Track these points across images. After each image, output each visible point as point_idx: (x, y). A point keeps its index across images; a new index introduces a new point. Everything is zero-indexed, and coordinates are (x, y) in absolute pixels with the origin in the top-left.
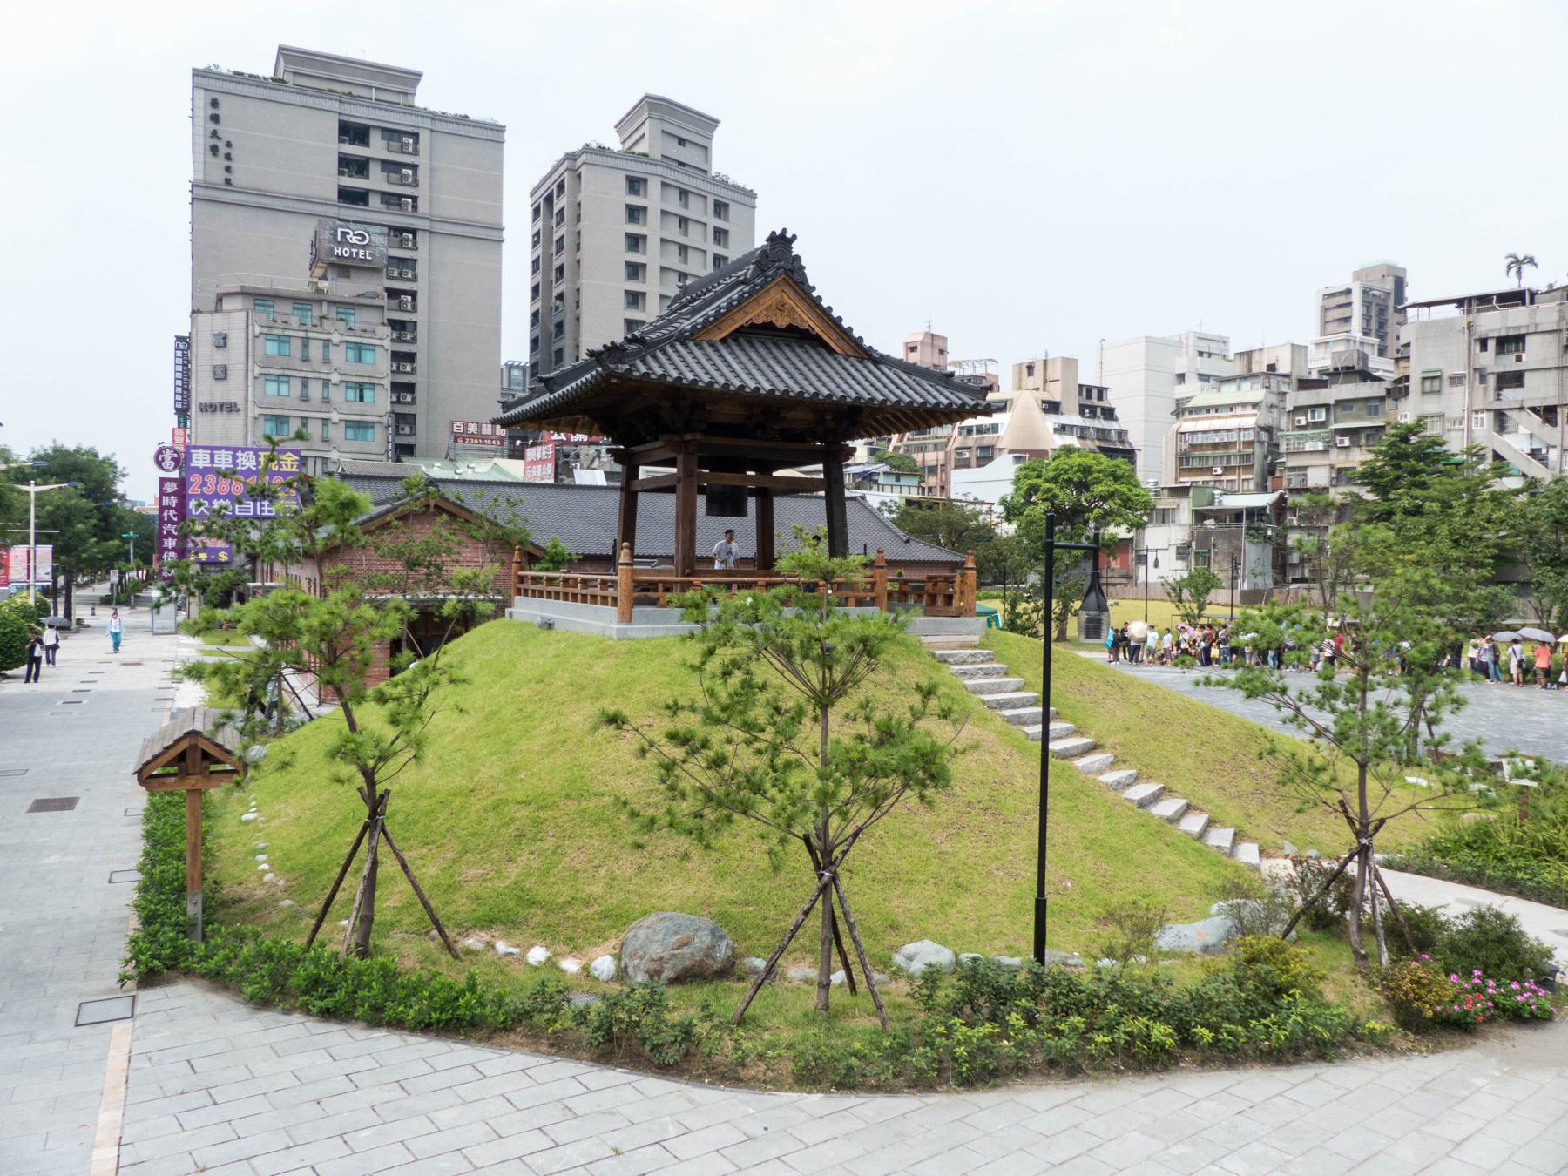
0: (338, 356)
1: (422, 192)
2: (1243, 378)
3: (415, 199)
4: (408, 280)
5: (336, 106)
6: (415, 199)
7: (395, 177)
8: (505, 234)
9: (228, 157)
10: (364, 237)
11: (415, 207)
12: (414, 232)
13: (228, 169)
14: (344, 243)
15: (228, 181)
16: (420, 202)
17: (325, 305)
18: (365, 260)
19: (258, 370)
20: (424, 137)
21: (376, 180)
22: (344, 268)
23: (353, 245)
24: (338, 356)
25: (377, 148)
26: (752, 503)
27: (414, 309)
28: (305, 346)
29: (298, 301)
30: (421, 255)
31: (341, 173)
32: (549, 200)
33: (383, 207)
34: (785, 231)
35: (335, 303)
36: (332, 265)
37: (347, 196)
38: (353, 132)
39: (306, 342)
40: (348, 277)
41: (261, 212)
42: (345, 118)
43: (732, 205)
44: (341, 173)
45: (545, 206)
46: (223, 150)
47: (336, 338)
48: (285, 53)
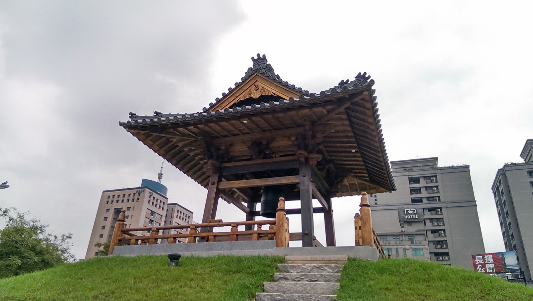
1: (441, 194)
3: (439, 197)
5: (407, 174)
6: (439, 197)
7: (430, 191)
10: (414, 211)
11: (439, 200)
12: (441, 208)
13: (376, 200)
14: (408, 214)
15: (376, 204)
16: (441, 197)
17: (404, 236)
18: (416, 219)
20: (439, 176)
21: (424, 194)
22: (409, 222)
23: (411, 214)
25: (423, 183)
27: (445, 236)
28: (397, 251)
29: (395, 236)
30: (444, 216)
31: (411, 194)
32: (498, 189)
33: (428, 202)
34: (365, 73)
35: (407, 235)
36: (405, 222)
37: (414, 201)
39: (397, 249)
40: (411, 225)
41: (387, 211)
44: (411, 194)
45: (496, 190)
47: (407, 247)
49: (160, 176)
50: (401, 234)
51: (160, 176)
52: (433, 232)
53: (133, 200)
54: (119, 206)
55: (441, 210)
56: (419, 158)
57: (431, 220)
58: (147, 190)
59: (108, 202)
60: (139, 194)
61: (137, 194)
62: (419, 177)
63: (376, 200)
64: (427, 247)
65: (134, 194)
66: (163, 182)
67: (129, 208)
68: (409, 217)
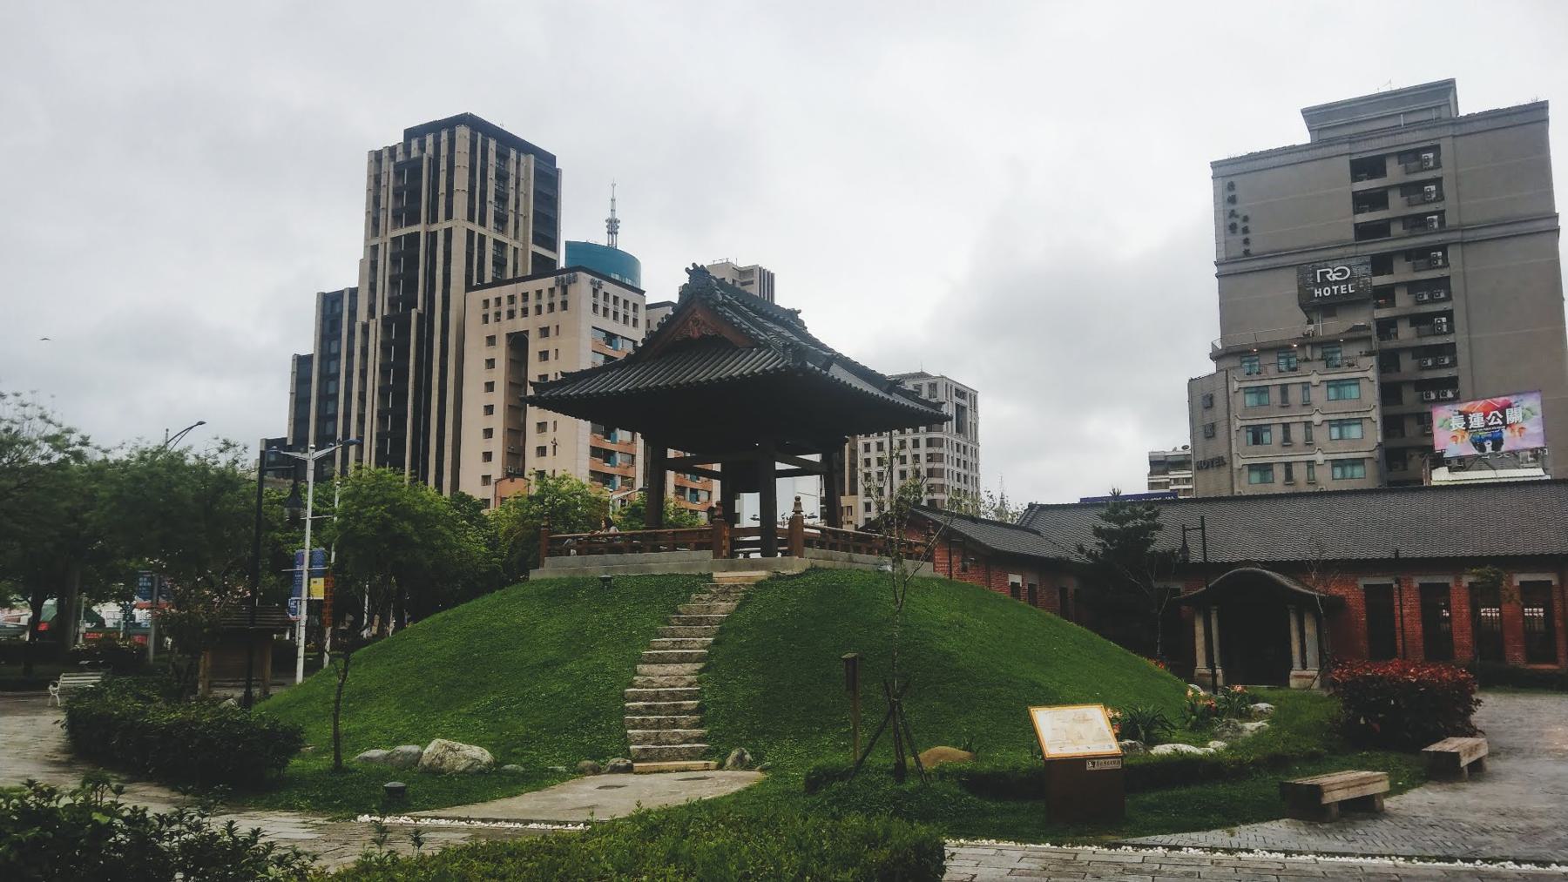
2: (517, 381)
3: (1441, 213)
5: (1346, 148)
6: (1441, 213)
7: (1416, 197)
8: (1215, 270)
9: (1246, 230)
11: (1442, 222)
12: (1443, 248)
13: (1246, 241)
14: (1326, 282)
19: (1239, 423)
20: (1446, 146)
21: (1397, 205)
22: (1329, 307)
23: (1336, 283)
24: (1318, 396)
25: (1395, 172)
31: (1356, 212)
42: (1355, 157)
46: (1240, 225)
47: (1315, 379)
48: (1313, 116)
49: (613, 227)
50: (1307, 341)
51: (613, 227)
53: (551, 307)
54: (519, 324)
55: (1445, 254)
56: (1396, 87)
57: (1412, 287)
58: (584, 278)
59: (486, 318)
60: (565, 292)
61: (558, 291)
63: (1246, 241)
64: (1372, 374)
65: (552, 290)
66: (624, 244)
67: (545, 332)
68: (1327, 292)
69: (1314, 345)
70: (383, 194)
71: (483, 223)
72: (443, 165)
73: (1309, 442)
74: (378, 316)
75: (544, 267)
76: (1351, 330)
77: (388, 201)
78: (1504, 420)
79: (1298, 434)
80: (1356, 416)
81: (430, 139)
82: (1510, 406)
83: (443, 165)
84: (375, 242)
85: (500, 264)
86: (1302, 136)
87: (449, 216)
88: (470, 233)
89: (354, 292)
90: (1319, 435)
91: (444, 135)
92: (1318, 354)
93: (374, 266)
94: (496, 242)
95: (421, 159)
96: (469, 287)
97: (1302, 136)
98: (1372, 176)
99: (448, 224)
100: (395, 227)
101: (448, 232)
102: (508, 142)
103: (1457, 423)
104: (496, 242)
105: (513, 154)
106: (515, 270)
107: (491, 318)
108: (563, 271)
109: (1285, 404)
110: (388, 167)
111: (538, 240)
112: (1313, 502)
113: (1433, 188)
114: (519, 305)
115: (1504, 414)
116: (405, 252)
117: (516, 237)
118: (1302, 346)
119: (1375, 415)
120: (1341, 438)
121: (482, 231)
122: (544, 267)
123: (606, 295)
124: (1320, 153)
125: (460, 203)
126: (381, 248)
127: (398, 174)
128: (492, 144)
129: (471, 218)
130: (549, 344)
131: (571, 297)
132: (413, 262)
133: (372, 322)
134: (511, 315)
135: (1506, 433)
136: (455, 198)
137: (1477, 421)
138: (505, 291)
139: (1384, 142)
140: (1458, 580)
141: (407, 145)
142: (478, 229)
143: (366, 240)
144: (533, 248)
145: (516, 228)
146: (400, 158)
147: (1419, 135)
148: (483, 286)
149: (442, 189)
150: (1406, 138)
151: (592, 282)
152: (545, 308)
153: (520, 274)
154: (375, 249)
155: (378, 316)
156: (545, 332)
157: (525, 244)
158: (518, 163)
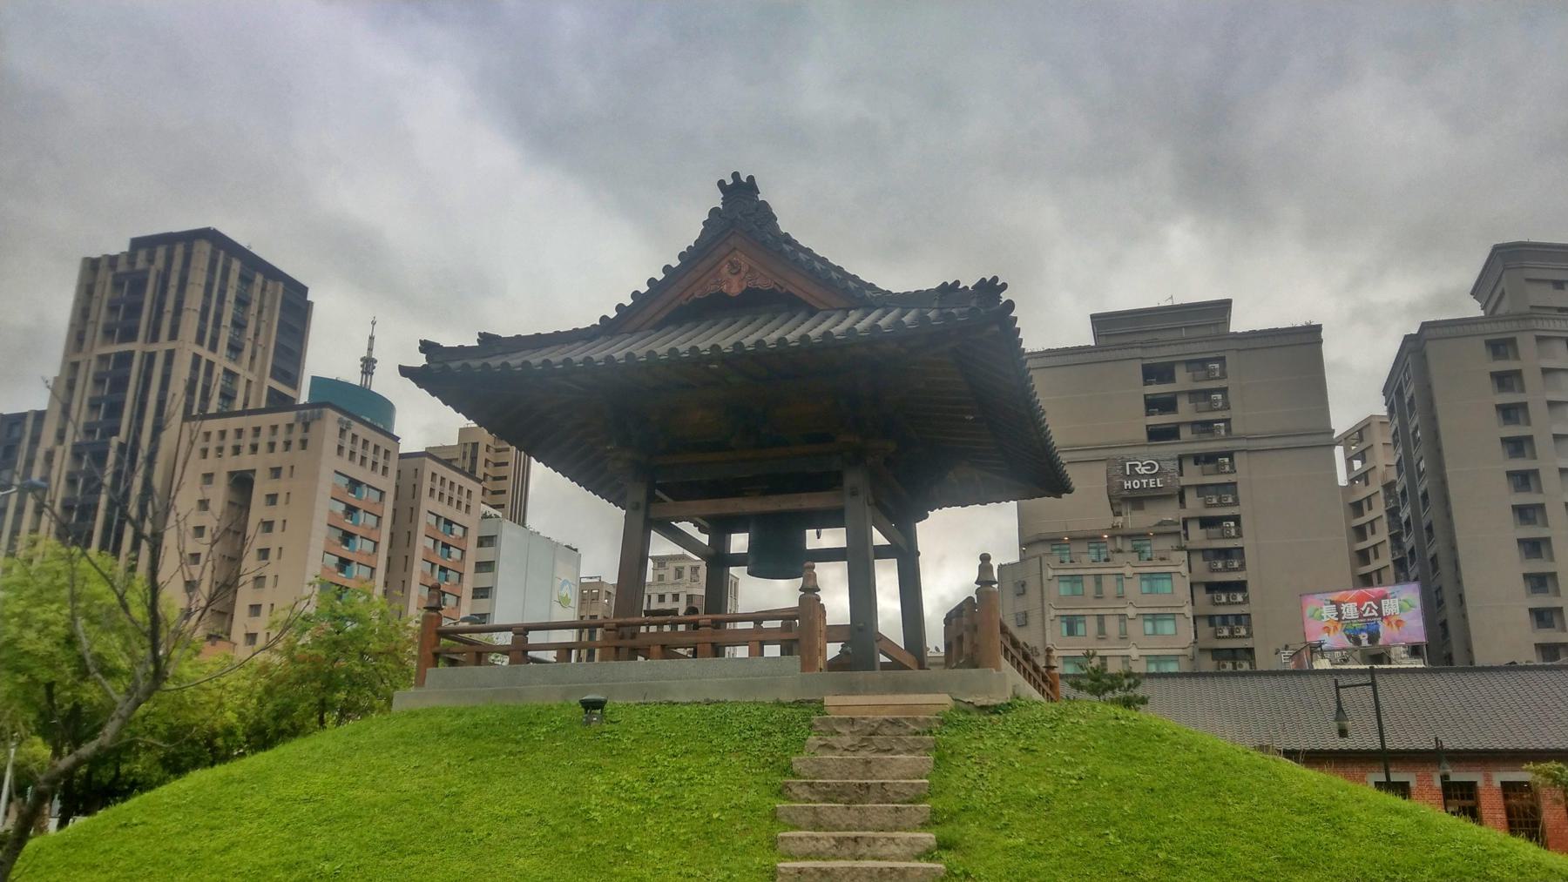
0: (1133, 588)
3: (1227, 421)
4: (1214, 506)
5: (1138, 352)
6: (1227, 421)
7: (1203, 405)
10: (1153, 467)
11: (1228, 430)
12: (1230, 455)
19: (1053, 613)
21: (1186, 411)
22: (1137, 500)
24: (1133, 588)
25: (1183, 380)
26: (935, 638)
38: (1152, 373)
43: (1519, 337)
47: (1128, 571)
48: (1100, 322)
50: (1116, 533)
52: (1206, 523)
53: (288, 444)
54: (245, 462)
55: (1231, 460)
57: (1201, 489)
58: (332, 416)
61: (298, 428)
62: (1173, 364)
64: (1184, 569)
65: (290, 426)
67: (276, 472)
68: (1136, 484)
69: (1124, 536)
70: (94, 307)
71: (213, 347)
72: (174, 281)
73: (1124, 637)
74: (68, 442)
75: (279, 402)
76: (1160, 524)
77: (100, 315)
78: (1379, 611)
79: (1112, 626)
80: (1169, 611)
81: (161, 252)
82: (1385, 597)
83: (174, 281)
84: (76, 358)
85: (228, 396)
86: (1086, 337)
87: (173, 336)
88: (197, 359)
89: (40, 416)
90: (1133, 628)
91: (179, 250)
92: (1128, 546)
93: (71, 386)
94: (227, 372)
95: (146, 272)
96: (187, 416)
97: (1086, 337)
98: (1161, 381)
99: (170, 346)
100: (104, 343)
101: (170, 355)
102: (254, 266)
103: (1328, 612)
104: (227, 372)
105: (259, 278)
106: (246, 404)
107: (212, 452)
108: (305, 406)
109: (1099, 596)
110: (106, 277)
111: (277, 373)
112: (1273, 681)
113: (1219, 396)
114: (247, 440)
115: (1379, 605)
116: (114, 376)
117: (251, 368)
118: (1113, 537)
119: (1188, 611)
120: (1155, 633)
121: (211, 357)
122: (279, 402)
123: (354, 437)
124: (1101, 356)
125: (190, 324)
126: (82, 369)
127: (118, 285)
128: (236, 265)
129: (200, 340)
130: (279, 486)
131: (312, 436)
132: (120, 384)
133: (59, 450)
134: (237, 450)
135: (1383, 627)
136: (185, 314)
137: (1350, 610)
138: (232, 424)
139: (1174, 350)
140: (1488, 779)
141: (131, 256)
142: (205, 354)
143: (66, 355)
144: (270, 382)
145: (253, 358)
146: (122, 267)
147: (1206, 346)
148: (205, 416)
149: (170, 305)
150: (1193, 348)
151: (340, 421)
152: (280, 445)
153: (250, 407)
154: (75, 366)
155: (68, 442)
156: (276, 472)
157: (261, 378)
158: (263, 289)
